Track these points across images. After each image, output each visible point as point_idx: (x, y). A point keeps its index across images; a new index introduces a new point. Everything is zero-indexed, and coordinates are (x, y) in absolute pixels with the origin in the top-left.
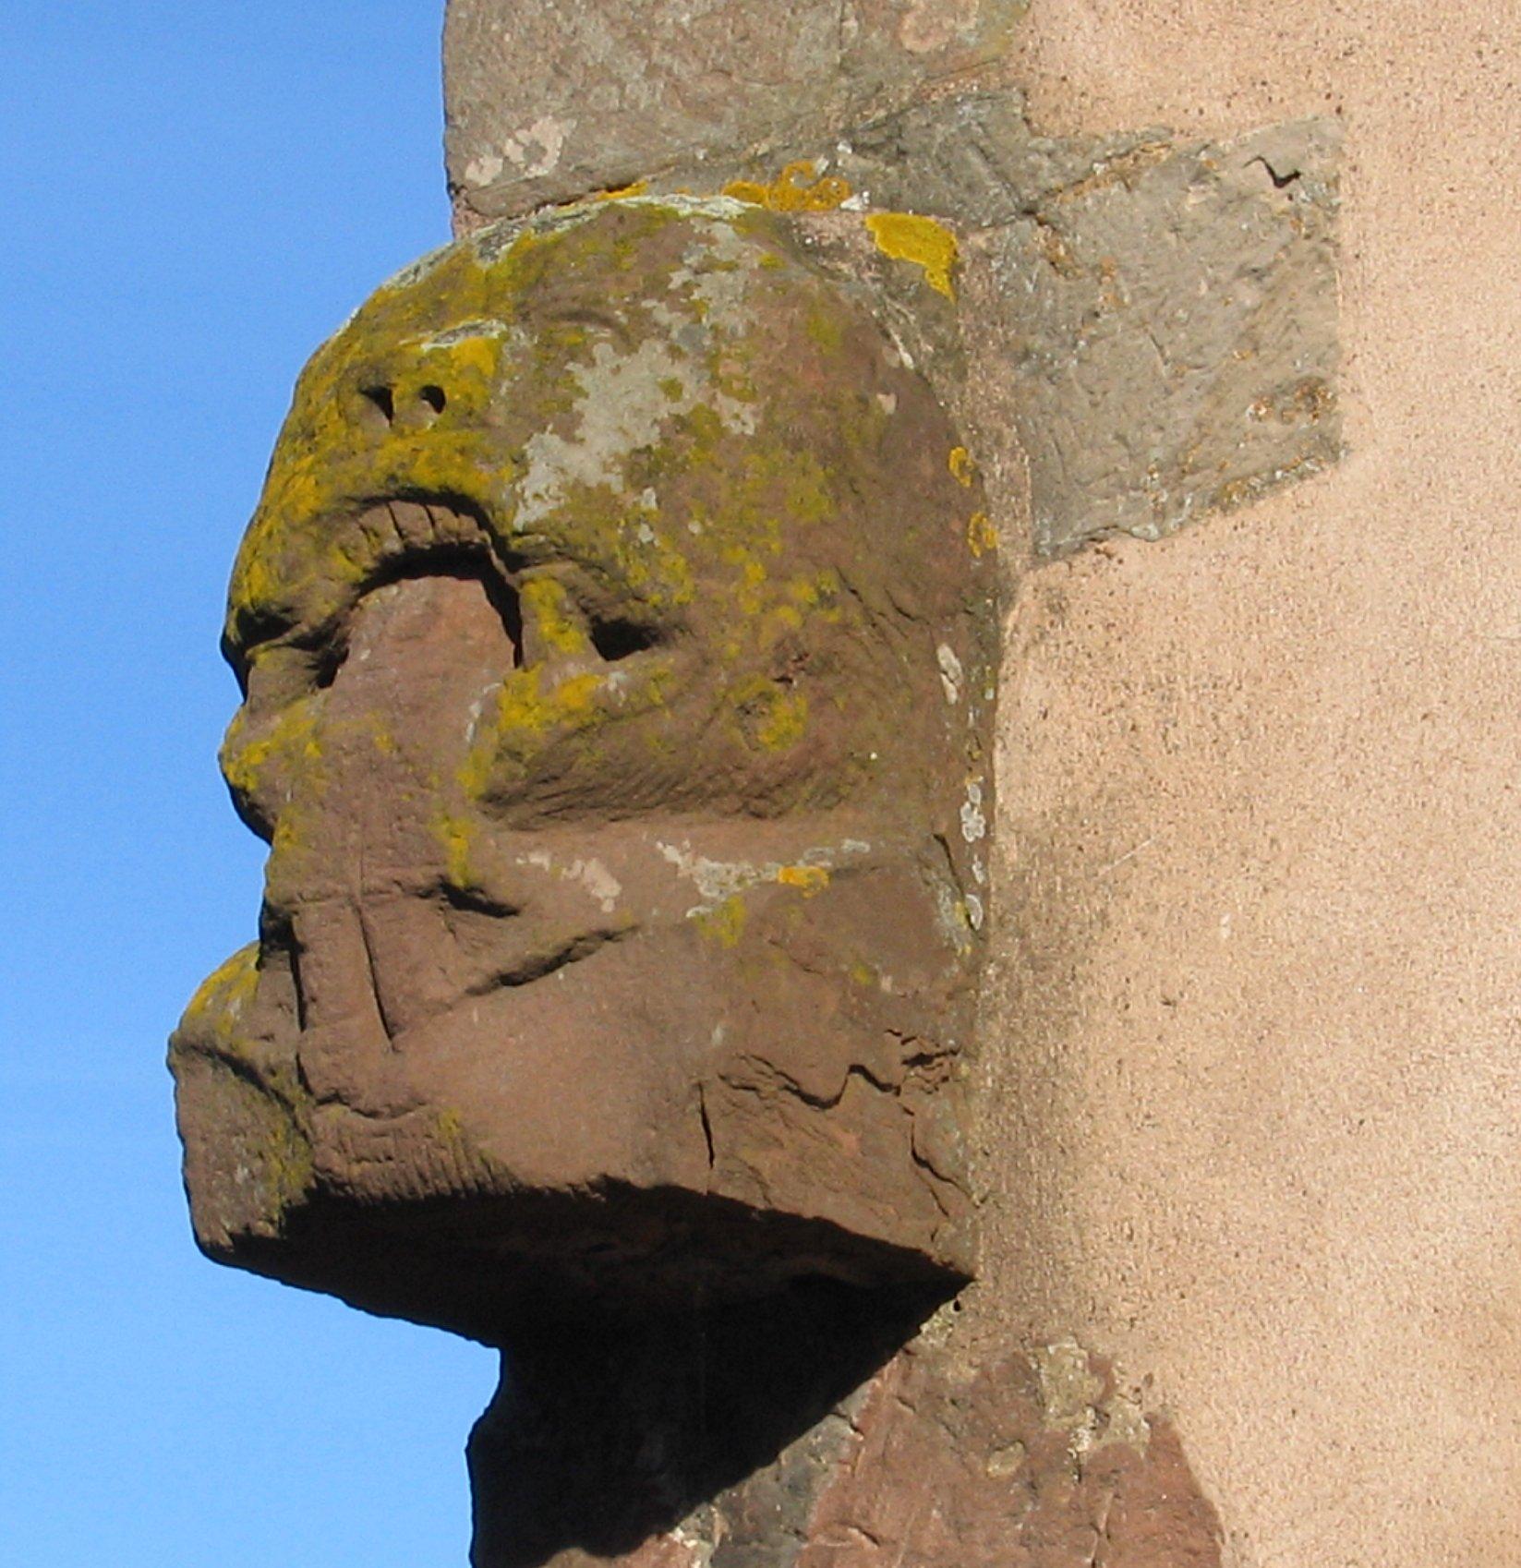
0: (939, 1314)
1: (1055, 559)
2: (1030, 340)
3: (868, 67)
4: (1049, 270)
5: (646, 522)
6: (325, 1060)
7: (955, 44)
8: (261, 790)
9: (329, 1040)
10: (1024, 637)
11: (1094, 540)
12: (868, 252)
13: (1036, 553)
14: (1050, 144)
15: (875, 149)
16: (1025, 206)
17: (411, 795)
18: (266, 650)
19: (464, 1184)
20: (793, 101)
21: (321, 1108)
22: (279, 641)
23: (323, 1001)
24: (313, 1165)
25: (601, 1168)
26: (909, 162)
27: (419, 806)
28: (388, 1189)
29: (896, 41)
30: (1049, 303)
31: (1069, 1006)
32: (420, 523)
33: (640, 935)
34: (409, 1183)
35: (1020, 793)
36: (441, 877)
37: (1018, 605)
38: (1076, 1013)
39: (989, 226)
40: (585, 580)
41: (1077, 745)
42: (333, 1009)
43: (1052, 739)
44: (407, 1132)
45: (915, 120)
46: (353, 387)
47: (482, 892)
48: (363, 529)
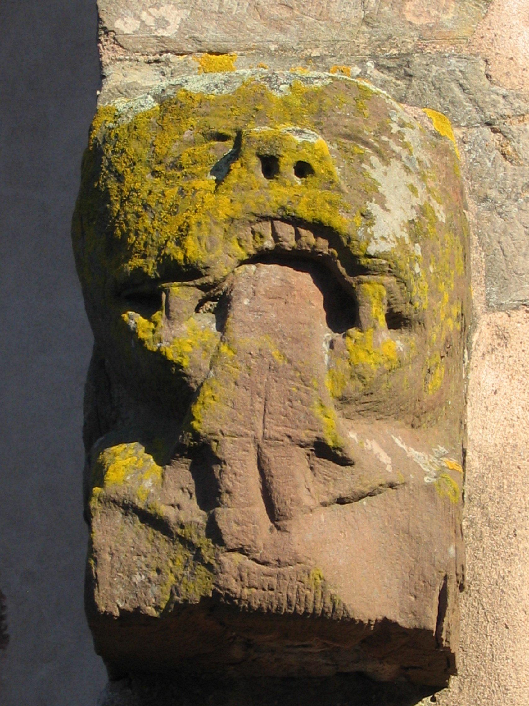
0: (423, 702)
1: (499, 310)
2: (489, 192)
3: (383, 25)
4: (501, 157)
5: (418, 262)
6: (235, 528)
7: (439, 25)
8: (191, 367)
9: (240, 517)
10: (482, 348)
11: (525, 305)
12: (430, 129)
13: (488, 305)
14: (503, 91)
15: (389, 69)
16: (488, 120)
17: (298, 389)
18: (179, 286)
19: (314, 609)
20: (334, 32)
21: (227, 554)
22: (191, 283)
23: (236, 494)
24: (217, 585)
25: (385, 614)
26: (413, 81)
27: (304, 396)
28: (264, 606)
29: (401, 15)
30: (501, 175)
31: (512, 550)
32: (290, 235)
33: (406, 488)
34: (280, 603)
35: (481, 431)
36: (317, 438)
37: (479, 331)
38: (516, 555)
39: (464, 126)
40: (396, 288)
41: (516, 412)
42: (242, 500)
43: (500, 406)
44: (288, 577)
45: (417, 59)
46: (254, 151)
47: (341, 450)
48: (253, 232)
